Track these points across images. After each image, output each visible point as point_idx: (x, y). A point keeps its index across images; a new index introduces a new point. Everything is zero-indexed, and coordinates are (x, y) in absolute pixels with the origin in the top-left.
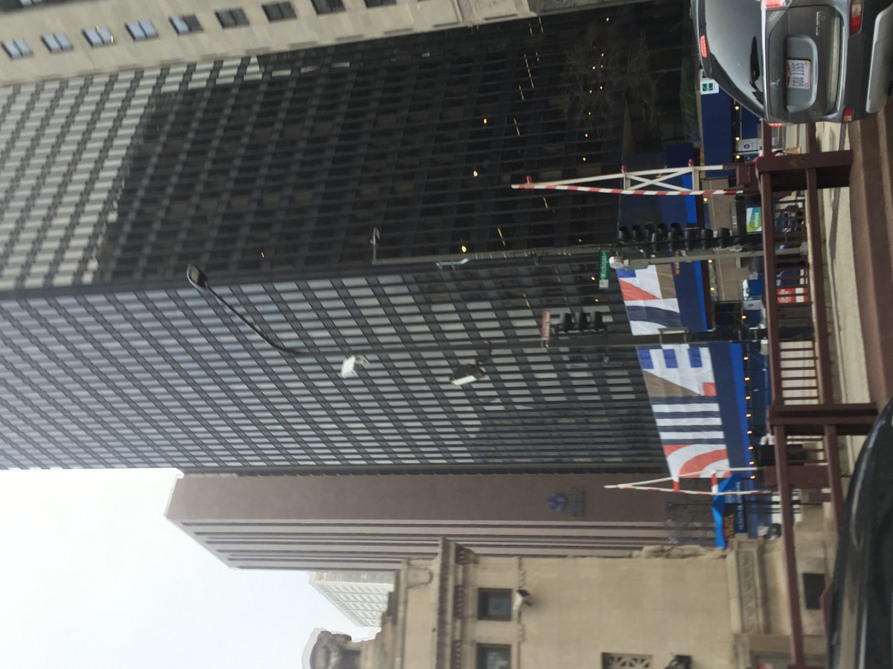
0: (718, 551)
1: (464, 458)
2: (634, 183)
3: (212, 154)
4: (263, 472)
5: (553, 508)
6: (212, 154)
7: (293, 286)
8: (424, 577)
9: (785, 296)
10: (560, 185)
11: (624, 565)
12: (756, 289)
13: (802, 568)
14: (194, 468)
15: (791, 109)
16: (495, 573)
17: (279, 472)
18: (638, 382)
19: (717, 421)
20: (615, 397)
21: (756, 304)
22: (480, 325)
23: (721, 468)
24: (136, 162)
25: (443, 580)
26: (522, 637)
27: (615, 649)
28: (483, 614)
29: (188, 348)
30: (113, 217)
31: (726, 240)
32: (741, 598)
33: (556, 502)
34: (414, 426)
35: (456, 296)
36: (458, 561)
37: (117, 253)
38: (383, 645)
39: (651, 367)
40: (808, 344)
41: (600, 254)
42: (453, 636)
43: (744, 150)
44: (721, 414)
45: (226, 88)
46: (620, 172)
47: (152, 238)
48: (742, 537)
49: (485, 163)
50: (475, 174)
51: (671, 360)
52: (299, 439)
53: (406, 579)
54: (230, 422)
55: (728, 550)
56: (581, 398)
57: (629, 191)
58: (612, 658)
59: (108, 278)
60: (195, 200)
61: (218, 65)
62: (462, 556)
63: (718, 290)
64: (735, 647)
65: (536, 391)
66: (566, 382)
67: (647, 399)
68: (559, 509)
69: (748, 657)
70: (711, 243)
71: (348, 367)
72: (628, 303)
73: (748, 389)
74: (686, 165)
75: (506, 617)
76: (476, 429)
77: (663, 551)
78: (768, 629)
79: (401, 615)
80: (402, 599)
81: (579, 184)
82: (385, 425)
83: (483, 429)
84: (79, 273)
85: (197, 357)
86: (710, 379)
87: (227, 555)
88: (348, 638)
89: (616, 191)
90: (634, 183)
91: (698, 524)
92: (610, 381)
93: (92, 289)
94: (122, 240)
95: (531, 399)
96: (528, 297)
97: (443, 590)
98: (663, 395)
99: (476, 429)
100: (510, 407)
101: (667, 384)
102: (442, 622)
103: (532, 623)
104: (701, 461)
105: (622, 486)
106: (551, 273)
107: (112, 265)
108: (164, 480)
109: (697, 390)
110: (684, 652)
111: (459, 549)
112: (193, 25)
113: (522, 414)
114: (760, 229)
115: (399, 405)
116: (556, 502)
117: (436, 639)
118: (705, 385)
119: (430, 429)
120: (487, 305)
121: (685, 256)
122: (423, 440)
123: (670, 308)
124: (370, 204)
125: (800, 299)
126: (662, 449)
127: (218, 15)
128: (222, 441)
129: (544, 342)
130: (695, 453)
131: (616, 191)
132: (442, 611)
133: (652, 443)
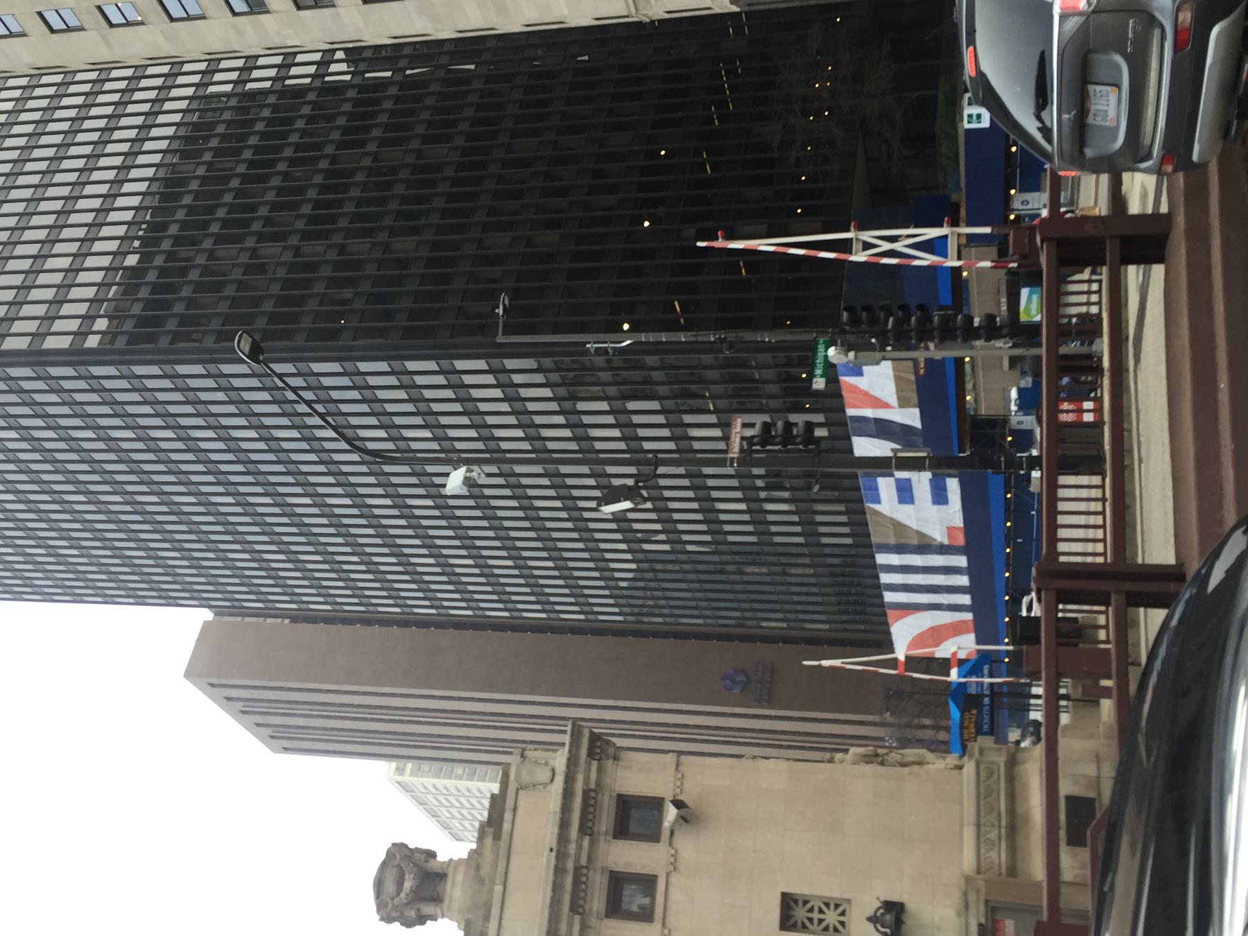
0: (952, 759)
1: (610, 613)
2: (867, 246)
3: (276, 181)
5: (728, 689)
6: (276, 181)
8: (546, 776)
9: (1067, 411)
10: (764, 245)
11: (821, 772)
12: (1028, 401)
13: (1066, 788)
14: (229, 609)
15: (1089, 153)
16: (643, 775)
17: (348, 620)
19: (964, 581)
20: (825, 540)
21: (1029, 421)
23: (965, 645)
24: (169, 186)
25: (569, 779)
26: (674, 866)
27: (799, 888)
28: (622, 831)
30: (132, 260)
31: (991, 330)
32: (978, 825)
33: (733, 681)
34: (542, 565)
35: (612, 391)
36: (591, 754)
37: (136, 309)
38: (478, 867)
39: (878, 501)
40: (1096, 480)
41: (815, 342)
42: (577, 860)
43: (1021, 207)
45: (299, 92)
46: (848, 230)
47: (186, 292)
48: (986, 741)
51: (905, 493)
52: (380, 576)
54: (284, 548)
55: (966, 758)
57: (859, 257)
58: (796, 901)
59: (121, 343)
63: (976, 400)
64: (965, 894)
67: (871, 546)
68: (736, 691)
69: (982, 908)
70: (970, 333)
71: (455, 481)
72: (851, 412)
73: (1009, 538)
74: (942, 226)
75: (654, 837)
76: (630, 575)
77: (877, 755)
78: (1012, 871)
79: (506, 826)
81: (793, 245)
82: (501, 564)
83: (639, 575)
84: (82, 334)
86: (959, 523)
87: (269, 731)
88: (431, 855)
89: (842, 256)
90: (867, 246)
91: (927, 722)
92: (819, 518)
94: (144, 293)
95: (708, 538)
96: (712, 397)
97: (568, 794)
98: (892, 541)
99: (630, 575)
100: (678, 547)
101: (898, 526)
102: (563, 838)
103: (687, 845)
104: (937, 635)
105: (826, 663)
107: (128, 326)
109: (939, 536)
110: (894, 897)
111: (594, 738)
114: (1038, 318)
115: (524, 537)
116: (733, 681)
117: (553, 862)
118: (951, 531)
120: (654, 405)
121: (933, 351)
122: (555, 586)
123: (908, 422)
125: (1088, 417)
126: (885, 615)
129: (732, 459)
130: (929, 623)
131: (842, 256)
132: (564, 825)
133: (869, 596)
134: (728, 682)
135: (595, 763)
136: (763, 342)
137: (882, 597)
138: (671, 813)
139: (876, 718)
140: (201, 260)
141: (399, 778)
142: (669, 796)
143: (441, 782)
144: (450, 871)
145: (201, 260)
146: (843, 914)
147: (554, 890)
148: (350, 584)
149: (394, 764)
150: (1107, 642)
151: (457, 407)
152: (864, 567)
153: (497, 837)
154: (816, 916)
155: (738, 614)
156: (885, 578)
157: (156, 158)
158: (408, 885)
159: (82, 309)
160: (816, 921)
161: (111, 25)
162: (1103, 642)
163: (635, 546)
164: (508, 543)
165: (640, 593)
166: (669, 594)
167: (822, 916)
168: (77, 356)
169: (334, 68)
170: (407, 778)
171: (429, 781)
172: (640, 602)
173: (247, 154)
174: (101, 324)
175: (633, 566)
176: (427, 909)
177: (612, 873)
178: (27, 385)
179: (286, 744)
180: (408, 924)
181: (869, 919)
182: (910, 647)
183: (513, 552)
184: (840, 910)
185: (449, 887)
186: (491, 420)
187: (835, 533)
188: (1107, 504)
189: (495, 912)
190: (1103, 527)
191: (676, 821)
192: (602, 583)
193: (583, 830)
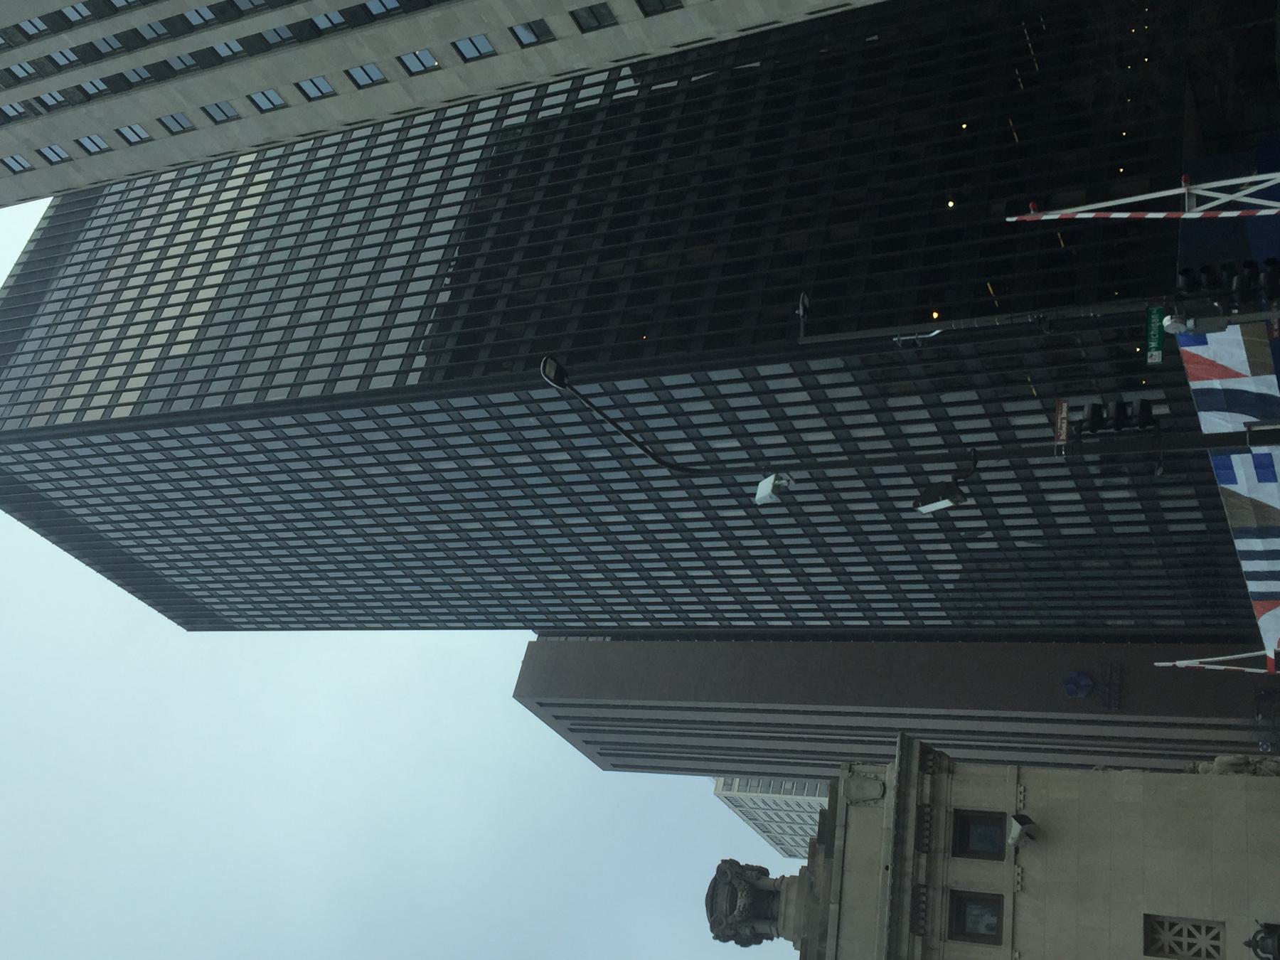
1: (936, 618)
3: (572, 204)
4: (646, 635)
7: (686, 378)
8: (874, 791)
10: (1083, 213)
16: (982, 788)
18: (1211, 498)
20: (1173, 528)
22: (960, 425)
24: (473, 221)
26: (1021, 885)
27: (1165, 910)
28: (961, 847)
29: (547, 469)
30: (444, 297)
34: (861, 570)
36: (923, 768)
37: (451, 344)
38: (812, 886)
39: (1233, 481)
41: (1149, 313)
42: (915, 878)
45: (589, 114)
46: (1180, 186)
47: (495, 323)
52: (696, 590)
53: (847, 791)
56: (1118, 530)
57: (1194, 214)
58: (1161, 924)
59: (438, 378)
60: (552, 268)
61: (578, 82)
62: (929, 761)
71: (764, 489)
72: (1195, 385)
75: (997, 853)
76: (956, 577)
77: (1248, 764)
79: (838, 843)
80: (840, 820)
82: (819, 571)
83: (965, 576)
84: (402, 373)
85: (556, 478)
88: (763, 872)
89: (1173, 215)
90: (1201, 200)
93: (419, 393)
96: (1034, 382)
97: (901, 809)
99: (956, 577)
103: (1034, 863)
107: (445, 361)
108: (511, 646)
111: (926, 750)
112: (542, 33)
115: (841, 541)
119: (884, 574)
120: (971, 395)
122: (875, 591)
123: (1264, 390)
126: (1251, 607)
127: (572, 14)
128: (592, 593)
129: (1060, 447)
131: (1173, 215)
132: (899, 841)
135: (928, 777)
136: (1089, 317)
137: (1239, 566)
138: (1015, 829)
139: (1247, 722)
140: (507, 290)
141: (728, 794)
142: (1011, 811)
143: (768, 797)
144: (783, 887)
145: (507, 290)
146: (1216, 937)
147: (892, 909)
148: (667, 599)
149: (722, 779)
151: (764, 414)
153: (829, 854)
154: (1185, 940)
155: (1078, 613)
156: (1247, 566)
157: (460, 197)
158: (740, 902)
159: (401, 348)
160: (1185, 946)
161: (411, 74)
163: (958, 545)
165: (968, 595)
166: (999, 594)
167: (1191, 940)
168: (398, 394)
169: (621, 85)
170: (735, 793)
171: (758, 796)
172: (969, 604)
173: (543, 182)
174: (420, 361)
175: (959, 567)
176: (762, 928)
177: (953, 892)
178: (358, 425)
179: (614, 760)
180: (744, 943)
181: (1248, 944)
183: (831, 559)
184: (1213, 933)
185: (783, 906)
186: (799, 424)
187: (1183, 515)
189: (832, 931)
191: (1020, 836)
193: (919, 847)
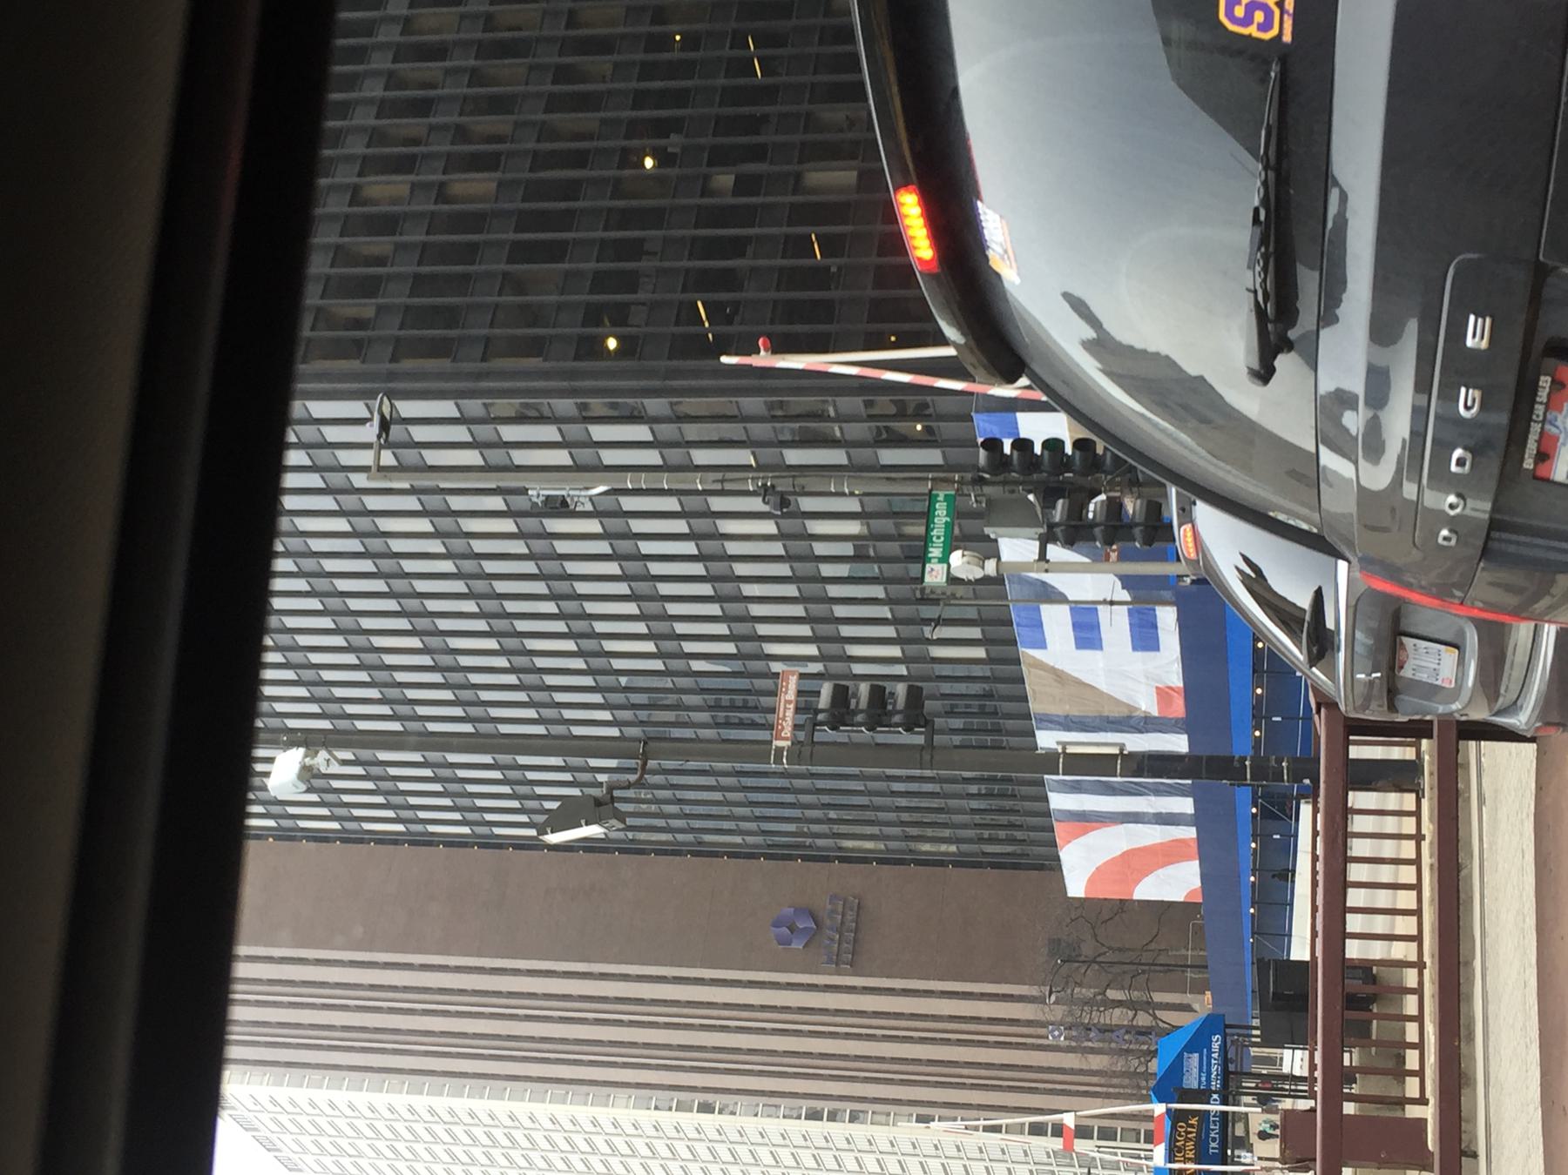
39: (1042, 645)
40: (1409, 801)
44: (1196, 820)
49: (674, 142)
50: (649, 163)
51: (1087, 632)
65: (727, 588)
66: (798, 547)
67: (1028, 716)
68: (798, 945)
86: (1176, 679)
95: (730, 648)
106: (820, 416)
109: (1147, 704)
113: (706, 683)
120: (641, 432)
124: (387, 224)
129: (779, 750)
133: (1024, 798)
134: (785, 930)
150: (1422, 1101)
152: (1010, 716)
162: (1414, 1101)
164: (346, 622)
166: (680, 794)
182: (1091, 881)
188: (1425, 845)
190: (1418, 938)
192: (511, 679)
